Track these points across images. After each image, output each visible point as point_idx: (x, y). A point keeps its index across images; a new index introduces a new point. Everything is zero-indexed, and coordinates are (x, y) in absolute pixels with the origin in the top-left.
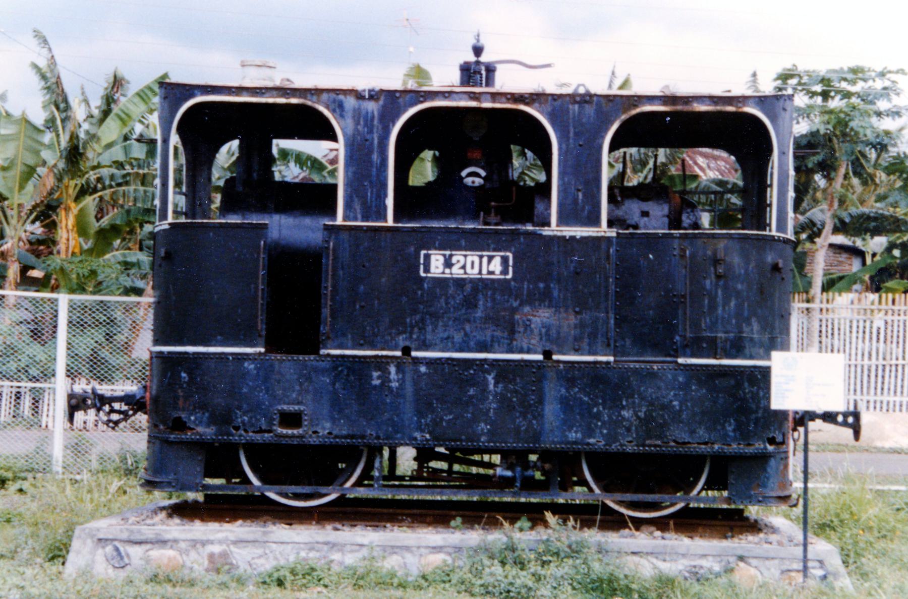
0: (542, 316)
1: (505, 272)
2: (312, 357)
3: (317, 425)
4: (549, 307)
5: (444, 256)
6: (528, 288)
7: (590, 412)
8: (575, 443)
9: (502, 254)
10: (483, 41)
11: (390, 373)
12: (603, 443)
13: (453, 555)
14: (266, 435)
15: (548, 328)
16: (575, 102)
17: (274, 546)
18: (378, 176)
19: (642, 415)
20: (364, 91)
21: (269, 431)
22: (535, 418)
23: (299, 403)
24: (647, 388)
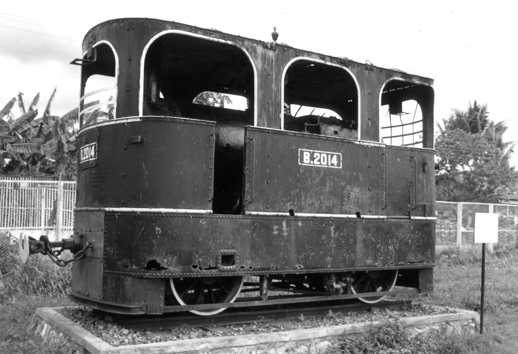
0: (355, 192)
1: (338, 165)
2: (240, 216)
3: (243, 262)
4: (358, 187)
5: (310, 152)
6: (349, 174)
7: (376, 246)
8: (370, 266)
9: (337, 153)
10: (277, 31)
11: (283, 227)
12: (381, 265)
13: (332, 341)
14: (213, 271)
15: (358, 199)
16: (367, 69)
17: (236, 349)
18: (276, 98)
19: (397, 248)
20: (268, 43)
21: (215, 268)
22: (352, 252)
23: (233, 248)
24: (399, 233)
